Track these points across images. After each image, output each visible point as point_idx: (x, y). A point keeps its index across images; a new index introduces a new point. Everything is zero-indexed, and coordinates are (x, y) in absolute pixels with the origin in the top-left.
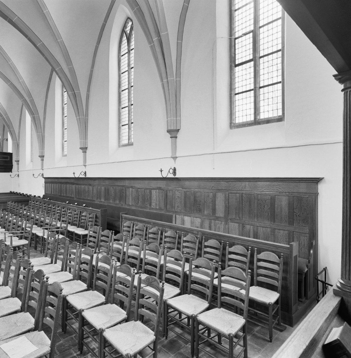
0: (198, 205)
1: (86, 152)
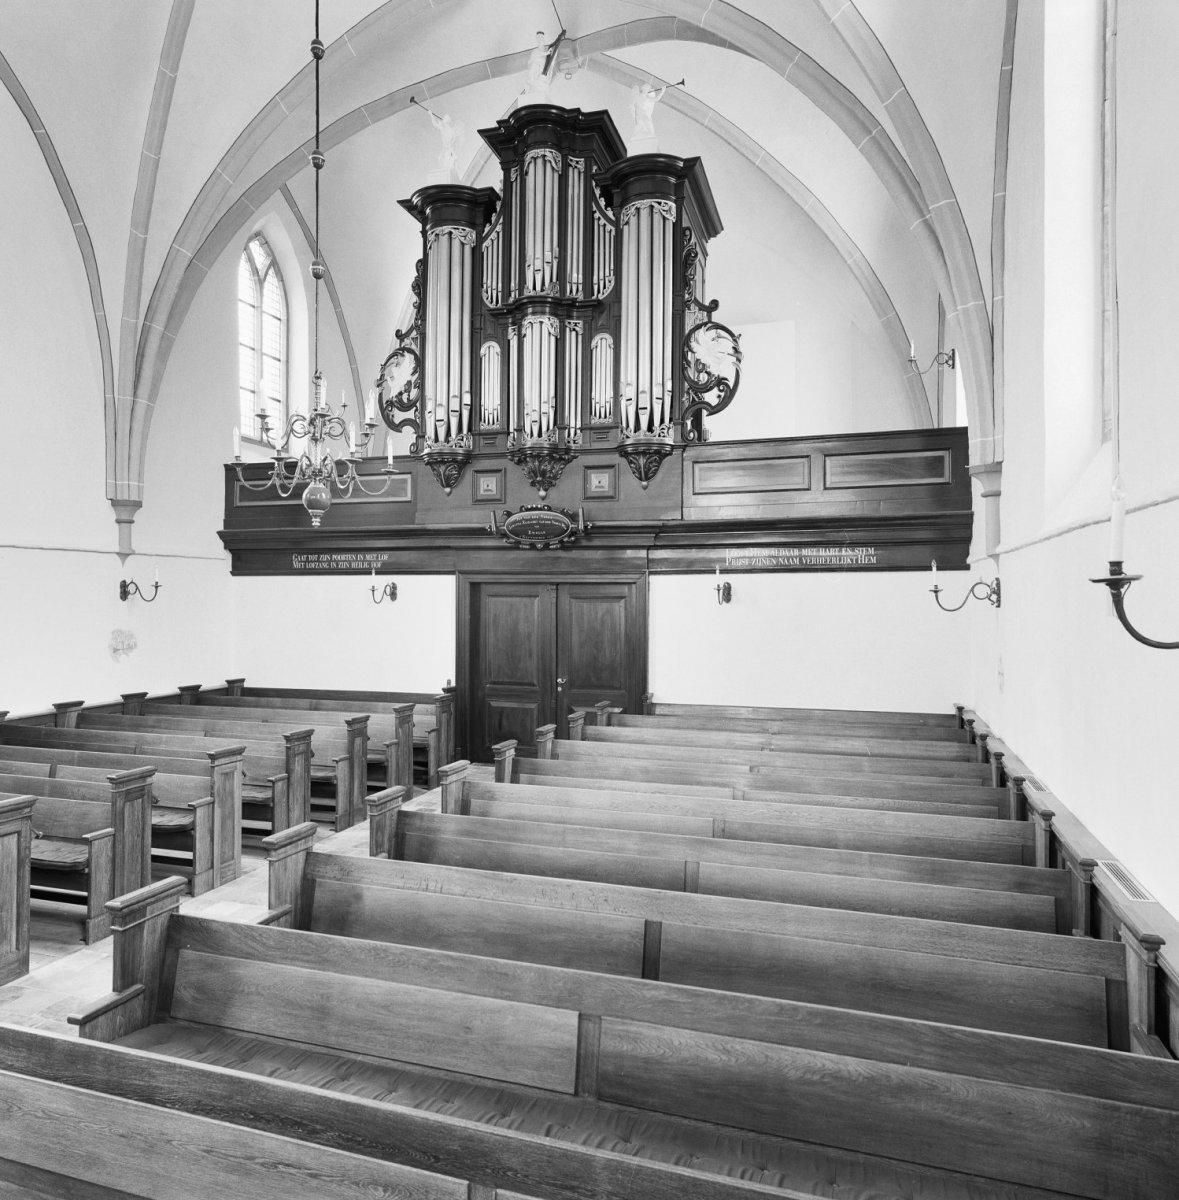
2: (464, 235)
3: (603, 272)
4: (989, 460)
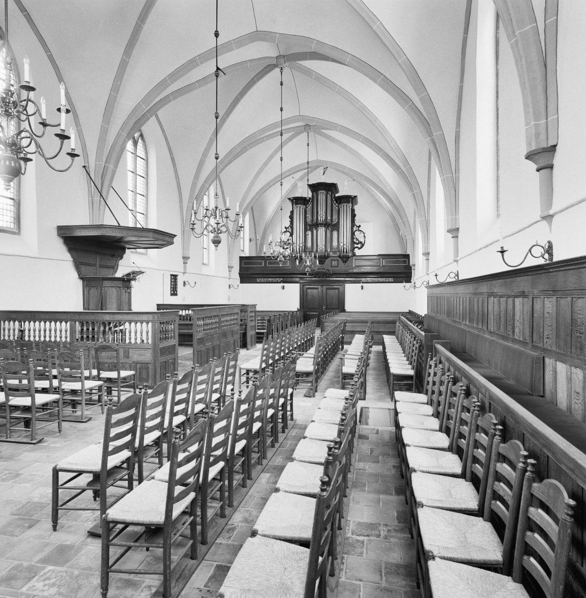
0: (578, 334)
1: (457, 237)
2: (302, 207)
3: (335, 217)
4: (427, 252)
